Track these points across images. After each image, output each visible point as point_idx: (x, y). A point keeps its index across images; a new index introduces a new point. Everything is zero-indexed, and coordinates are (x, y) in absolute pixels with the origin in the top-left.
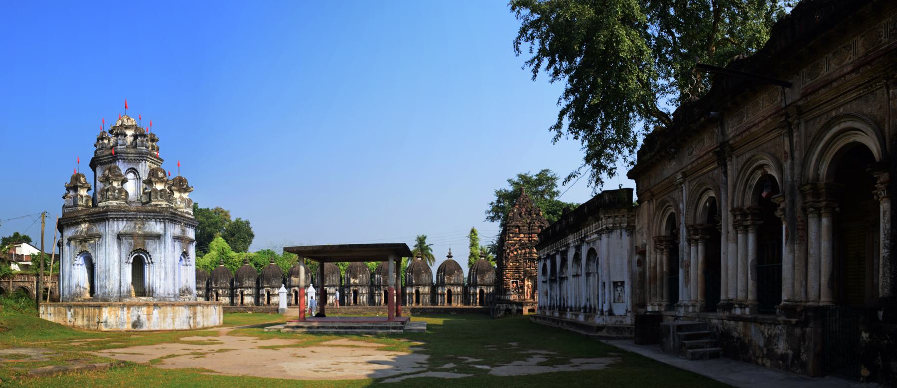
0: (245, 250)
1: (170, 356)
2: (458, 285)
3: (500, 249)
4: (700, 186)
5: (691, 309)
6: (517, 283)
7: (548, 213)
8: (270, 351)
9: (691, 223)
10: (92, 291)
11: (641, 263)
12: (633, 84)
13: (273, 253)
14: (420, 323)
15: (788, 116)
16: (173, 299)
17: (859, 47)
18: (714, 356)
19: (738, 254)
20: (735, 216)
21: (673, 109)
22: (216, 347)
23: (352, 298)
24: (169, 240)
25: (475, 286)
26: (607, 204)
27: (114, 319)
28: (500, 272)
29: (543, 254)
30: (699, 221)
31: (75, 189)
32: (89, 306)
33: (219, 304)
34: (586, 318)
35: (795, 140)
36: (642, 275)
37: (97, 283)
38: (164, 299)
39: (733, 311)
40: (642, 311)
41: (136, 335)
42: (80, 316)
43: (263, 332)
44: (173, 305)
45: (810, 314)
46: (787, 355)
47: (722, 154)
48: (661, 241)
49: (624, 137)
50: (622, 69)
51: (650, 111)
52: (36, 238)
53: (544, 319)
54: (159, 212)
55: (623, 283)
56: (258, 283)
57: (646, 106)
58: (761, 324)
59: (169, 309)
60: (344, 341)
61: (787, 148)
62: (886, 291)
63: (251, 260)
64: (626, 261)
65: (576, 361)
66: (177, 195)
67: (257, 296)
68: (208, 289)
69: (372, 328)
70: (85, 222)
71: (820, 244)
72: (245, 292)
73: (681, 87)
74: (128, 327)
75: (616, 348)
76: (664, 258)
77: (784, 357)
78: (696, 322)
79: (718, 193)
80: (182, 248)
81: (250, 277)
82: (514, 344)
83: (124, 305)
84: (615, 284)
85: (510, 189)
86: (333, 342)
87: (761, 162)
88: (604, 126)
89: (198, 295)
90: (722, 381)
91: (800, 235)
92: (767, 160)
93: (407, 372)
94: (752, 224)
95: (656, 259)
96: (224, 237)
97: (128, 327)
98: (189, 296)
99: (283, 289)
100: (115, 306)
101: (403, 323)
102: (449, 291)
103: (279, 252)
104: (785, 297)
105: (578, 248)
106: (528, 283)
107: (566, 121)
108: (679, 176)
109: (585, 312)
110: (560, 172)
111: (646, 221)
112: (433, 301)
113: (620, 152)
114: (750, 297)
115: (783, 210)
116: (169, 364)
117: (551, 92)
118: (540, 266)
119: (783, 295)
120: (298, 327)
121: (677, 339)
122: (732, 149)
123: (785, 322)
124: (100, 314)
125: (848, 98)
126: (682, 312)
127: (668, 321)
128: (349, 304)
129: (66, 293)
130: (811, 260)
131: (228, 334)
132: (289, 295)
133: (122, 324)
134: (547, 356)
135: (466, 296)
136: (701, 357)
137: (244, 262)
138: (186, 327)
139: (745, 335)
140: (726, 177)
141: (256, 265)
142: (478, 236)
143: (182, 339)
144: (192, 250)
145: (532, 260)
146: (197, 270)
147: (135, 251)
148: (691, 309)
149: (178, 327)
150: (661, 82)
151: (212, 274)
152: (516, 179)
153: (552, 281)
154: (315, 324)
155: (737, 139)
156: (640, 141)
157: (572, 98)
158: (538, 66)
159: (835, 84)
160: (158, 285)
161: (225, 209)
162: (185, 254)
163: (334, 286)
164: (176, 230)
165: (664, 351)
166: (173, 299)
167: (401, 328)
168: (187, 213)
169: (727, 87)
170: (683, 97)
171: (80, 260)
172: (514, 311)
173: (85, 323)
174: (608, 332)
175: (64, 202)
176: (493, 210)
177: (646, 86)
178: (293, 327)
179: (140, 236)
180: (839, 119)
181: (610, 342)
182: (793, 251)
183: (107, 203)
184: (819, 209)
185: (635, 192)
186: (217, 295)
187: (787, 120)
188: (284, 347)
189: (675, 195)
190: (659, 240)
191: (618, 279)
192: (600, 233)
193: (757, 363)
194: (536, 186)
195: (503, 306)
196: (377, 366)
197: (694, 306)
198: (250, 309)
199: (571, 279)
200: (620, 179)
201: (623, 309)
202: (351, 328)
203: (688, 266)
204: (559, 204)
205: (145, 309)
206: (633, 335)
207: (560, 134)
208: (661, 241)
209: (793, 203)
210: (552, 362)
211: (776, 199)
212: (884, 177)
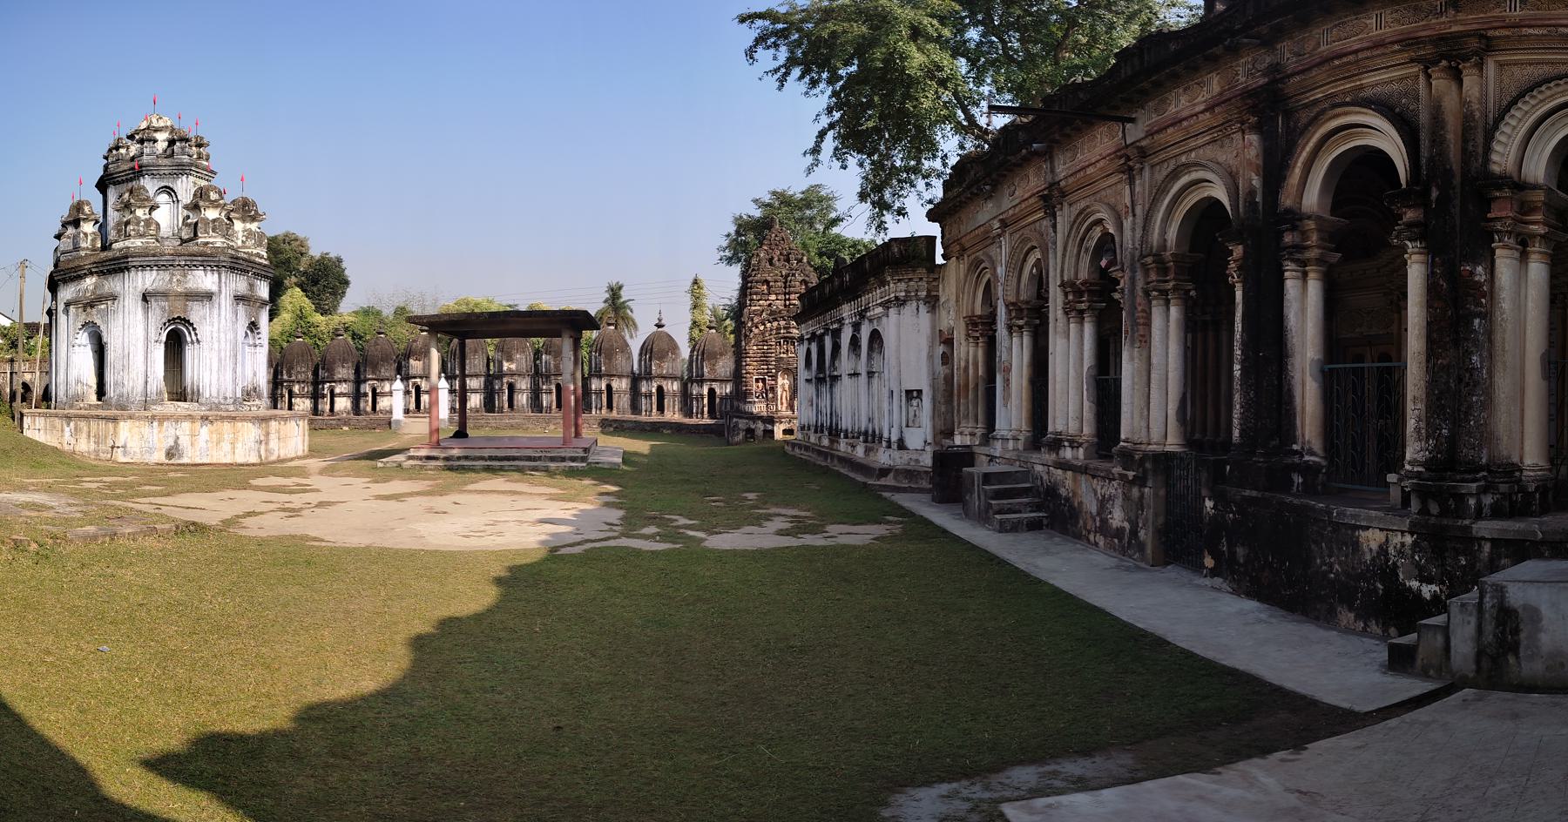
2: (674, 378)
6: (764, 380)
7: (821, 255)
8: (392, 503)
9: (1012, 299)
10: (101, 392)
11: (947, 359)
13: (379, 313)
14: (612, 448)
15: (1128, 159)
16: (231, 408)
18: (1034, 526)
19: (1071, 350)
20: (1066, 294)
22: (313, 498)
23: (506, 397)
24: (225, 301)
25: (701, 382)
27: (139, 442)
32: (98, 417)
34: (867, 451)
36: (949, 380)
37: (110, 378)
38: (217, 407)
39: (1061, 452)
41: (177, 474)
42: (84, 435)
43: (376, 468)
44: (234, 418)
46: (1123, 529)
47: (1051, 200)
53: (807, 448)
54: (211, 255)
56: (357, 372)
58: (1094, 477)
59: (227, 426)
60: (498, 483)
61: (1128, 201)
65: (833, 529)
66: (238, 226)
67: (357, 397)
70: (92, 274)
72: (337, 390)
74: (160, 456)
75: (902, 507)
76: (980, 352)
77: (1119, 532)
79: (1045, 252)
80: (249, 315)
81: (345, 361)
82: (751, 496)
83: (153, 418)
84: (909, 392)
86: (481, 486)
87: (1099, 216)
90: (1022, 567)
93: (593, 537)
95: (967, 352)
96: (301, 286)
97: (160, 456)
98: (257, 402)
99: (398, 385)
100: (139, 419)
101: (586, 450)
102: (660, 389)
103: (388, 312)
105: (856, 327)
106: (783, 382)
107: (829, 144)
108: (997, 225)
109: (866, 441)
112: (635, 408)
114: (1086, 430)
117: (807, 107)
120: (429, 458)
122: (1063, 194)
123: (1122, 477)
124: (115, 433)
125: (1200, 141)
126: (997, 449)
128: (501, 410)
129: (61, 393)
132: (407, 392)
133: (151, 451)
135: (686, 400)
136: (1014, 528)
137: (336, 333)
138: (254, 459)
139: (1075, 494)
141: (354, 336)
143: (254, 482)
145: (789, 340)
147: (172, 321)
148: (1011, 444)
151: (283, 357)
152: (767, 199)
153: (820, 381)
154: (456, 452)
155: (1071, 180)
157: (837, 115)
158: (787, 74)
160: (207, 381)
161: (301, 235)
162: (253, 326)
163: (477, 376)
164: (239, 284)
165: (967, 515)
166: (231, 408)
167: (583, 459)
168: (258, 255)
171: (84, 338)
172: (759, 432)
173: (93, 446)
174: (895, 478)
178: (420, 458)
179: (180, 295)
180: (1188, 167)
185: (939, 241)
187: (1130, 161)
188: (411, 494)
189: (993, 250)
190: (971, 322)
192: (886, 305)
194: (800, 209)
195: (742, 424)
197: (1015, 439)
199: (845, 379)
201: (919, 437)
203: (1008, 370)
204: (841, 241)
205: (186, 425)
207: (817, 163)
208: (975, 324)
209: (1133, 280)
210: (799, 528)
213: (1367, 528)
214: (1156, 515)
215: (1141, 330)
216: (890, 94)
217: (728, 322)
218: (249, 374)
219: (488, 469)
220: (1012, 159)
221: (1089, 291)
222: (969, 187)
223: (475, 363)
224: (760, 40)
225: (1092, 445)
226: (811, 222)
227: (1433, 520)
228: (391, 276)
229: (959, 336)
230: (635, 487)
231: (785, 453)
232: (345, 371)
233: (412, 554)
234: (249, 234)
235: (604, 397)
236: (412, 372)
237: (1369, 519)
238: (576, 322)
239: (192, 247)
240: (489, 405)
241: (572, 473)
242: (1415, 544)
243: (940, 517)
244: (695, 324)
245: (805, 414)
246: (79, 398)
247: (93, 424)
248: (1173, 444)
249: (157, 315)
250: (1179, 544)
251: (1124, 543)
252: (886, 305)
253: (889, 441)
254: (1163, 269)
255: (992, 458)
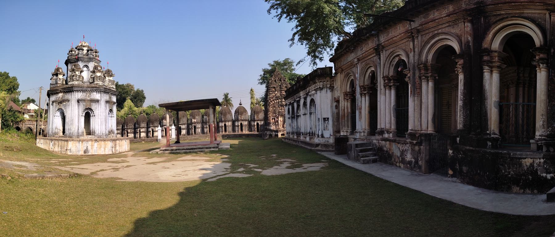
0: (141, 106)
1: (101, 170)
2: (246, 120)
3: (265, 100)
4: (367, 65)
5: (362, 134)
7: (290, 80)
8: (152, 166)
9: (362, 84)
10: (64, 132)
11: (337, 107)
12: (331, 22)
13: (155, 107)
14: (226, 144)
15: (412, 33)
17: (451, 8)
18: (374, 161)
19: (386, 101)
20: (385, 81)
21: (352, 31)
22: (125, 164)
24: (103, 103)
25: (254, 121)
26: (320, 75)
27: (75, 148)
28: (266, 112)
29: (288, 102)
30: (366, 83)
31: (57, 75)
33: (127, 139)
34: (310, 139)
35: (415, 43)
36: (338, 114)
37: (66, 127)
39: (384, 135)
40: (338, 135)
42: (57, 146)
45: (423, 138)
46: (411, 161)
47: (378, 50)
48: (347, 95)
49: (327, 43)
50: (325, 17)
51: (340, 31)
52: (37, 102)
53: (289, 140)
55: (328, 118)
56: (147, 125)
57: (338, 30)
58: (398, 143)
59: (103, 142)
60: (189, 157)
61: (411, 47)
62: (461, 126)
63: (144, 112)
64: (329, 106)
65: (305, 165)
66: (107, 78)
67: (147, 132)
68: (123, 129)
69: (202, 148)
71: (428, 97)
72: (141, 131)
73: (356, 23)
74: (82, 153)
75: (325, 157)
77: (410, 163)
78: (365, 142)
79: (376, 67)
80: (110, 107)
81: (143, 121)
82: (274, 155)
83: (80, 140)
84: (324, 119)
85: (270, 68)
88: (317, 39)
89: (117, 134)
90: (378, 176)
91: (418, 92)
92: (401, 52)
93: (219, 174)
94: (393, 85)
95: (345, 105)
96: (131, 99)
97: (82, 153)
99: (159, 128)
100: (75, 141)
101: (218, 144)
102: (241, 124)
104: (410, 128)
105: (305, 98)
106: (281, 119)
107: (297, 37)
108: (356, 60)
109: (310, 135)
110: (295, 59)
111: (339, 84)
112: (234, 130)
113: (325, 50)
115: (409, 77)
116: (100, 175)
117: (290, 26)
118: (286, 108)
119: (409, 126)
120: (166, 150)
121: (356, 152)
122: (383, 47)
123: (411, 143)
125: (444, 26)
126: (357, 136)
127: (351, 142)
128: (192, 134)
130: (423, 106)
131: (133, 156)
132: (162, 131)
133: (79, 151)
134: (291, 163)
135: (250, 127)
138: (111, 153)
139: (390, 149)
140: (380, 60)
141: (147, 114)
142: (255, 93)
143: (108, 160)
144: (115, 108)
145: (282, 106)
146: (117, 119)
147: (86, 109)
148: (362, 134)
149: (107, 153)
150: (346, 21)
151: (125, 121)
152: (272, 63)
154: (174, 148)
156: (336, 44)
157: (299, 28)
158: (281, 17)
159: (437, 21)
161: (132, 84)
162: (111, 111)
163: (184, 124)
164: (106, 97)
165: (349, 158)
167: (217, 147)
168: (112, 88)
169: (378, 24)
170: (358, 26)
172: (273, 135)
173: (60, 149)
175: (51, 82)
176: (261, 79)
177: (339, 22)
178: (163, 150)
179: (88, 100)
180: (438, 34)
181: (323, 153)
182: (414, 101)
183: (73, 83)
184: (428, 77)
185: (333, 68)
186: (128, 133)
187: (411, 35)
189: (354, 69)
190: (346, 94)
191: (325, 116)
192: (316, 90)
193: (396, 166)
195: (268, 133)
196: (204, 172)
197: (364, 132)
198: (144, 140)
199: (302, 116)
200: (325, 62)
201: (328, 133)
202: (192, 149)
203: (361, 109)
204: (295, 75)
205: (90, 143)
206: (334, 149)
207: (293, 43)
208: (347, 95)
209: (414, 74)
210: (293, 166)
211: (406, 72)
212: (461, 62)
213: (525, 158)
214: (426, 156)
215: (418, 90)
216: (319, 20)
217: (261, 103)
218: (110, 126)
219: (186, 153)
220: (363, 38)
221: (394, 79)
222: (345, 49)
223: (183, 120)
224: (272, 7)
225: (395, 132)
226: (286, 70)
227: (552, 153)
228: (157, 94)
229: (342, 99)
230: (235, 156)
231: (282, 142)
232: (143, 125)
233: (153, 184)
234: (110, 81)
235: (224, 128)
236: (164, 124)
237: (527, 155)
238: (214, 103)
239: (93, 85)
240: (188, 133)
241: (212, 152)
242: (545, 162)
243: (340, 159)
244: (252, 103)
245: (288, 129)
246: (56, 133)
247: (60, 142)
248: (430, 130)
249: (82, 107)
250: (436, 166)
251: (413, 167)
252: (316, 90)
253: (318, 135)
254: (426, 69)
255: (355, 139)
